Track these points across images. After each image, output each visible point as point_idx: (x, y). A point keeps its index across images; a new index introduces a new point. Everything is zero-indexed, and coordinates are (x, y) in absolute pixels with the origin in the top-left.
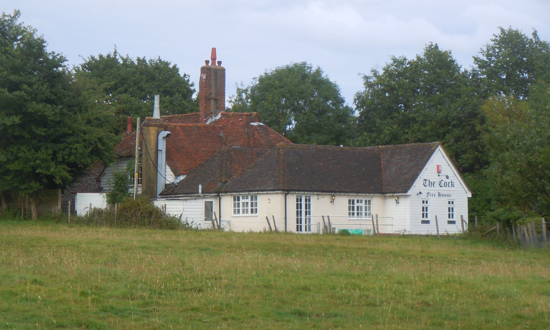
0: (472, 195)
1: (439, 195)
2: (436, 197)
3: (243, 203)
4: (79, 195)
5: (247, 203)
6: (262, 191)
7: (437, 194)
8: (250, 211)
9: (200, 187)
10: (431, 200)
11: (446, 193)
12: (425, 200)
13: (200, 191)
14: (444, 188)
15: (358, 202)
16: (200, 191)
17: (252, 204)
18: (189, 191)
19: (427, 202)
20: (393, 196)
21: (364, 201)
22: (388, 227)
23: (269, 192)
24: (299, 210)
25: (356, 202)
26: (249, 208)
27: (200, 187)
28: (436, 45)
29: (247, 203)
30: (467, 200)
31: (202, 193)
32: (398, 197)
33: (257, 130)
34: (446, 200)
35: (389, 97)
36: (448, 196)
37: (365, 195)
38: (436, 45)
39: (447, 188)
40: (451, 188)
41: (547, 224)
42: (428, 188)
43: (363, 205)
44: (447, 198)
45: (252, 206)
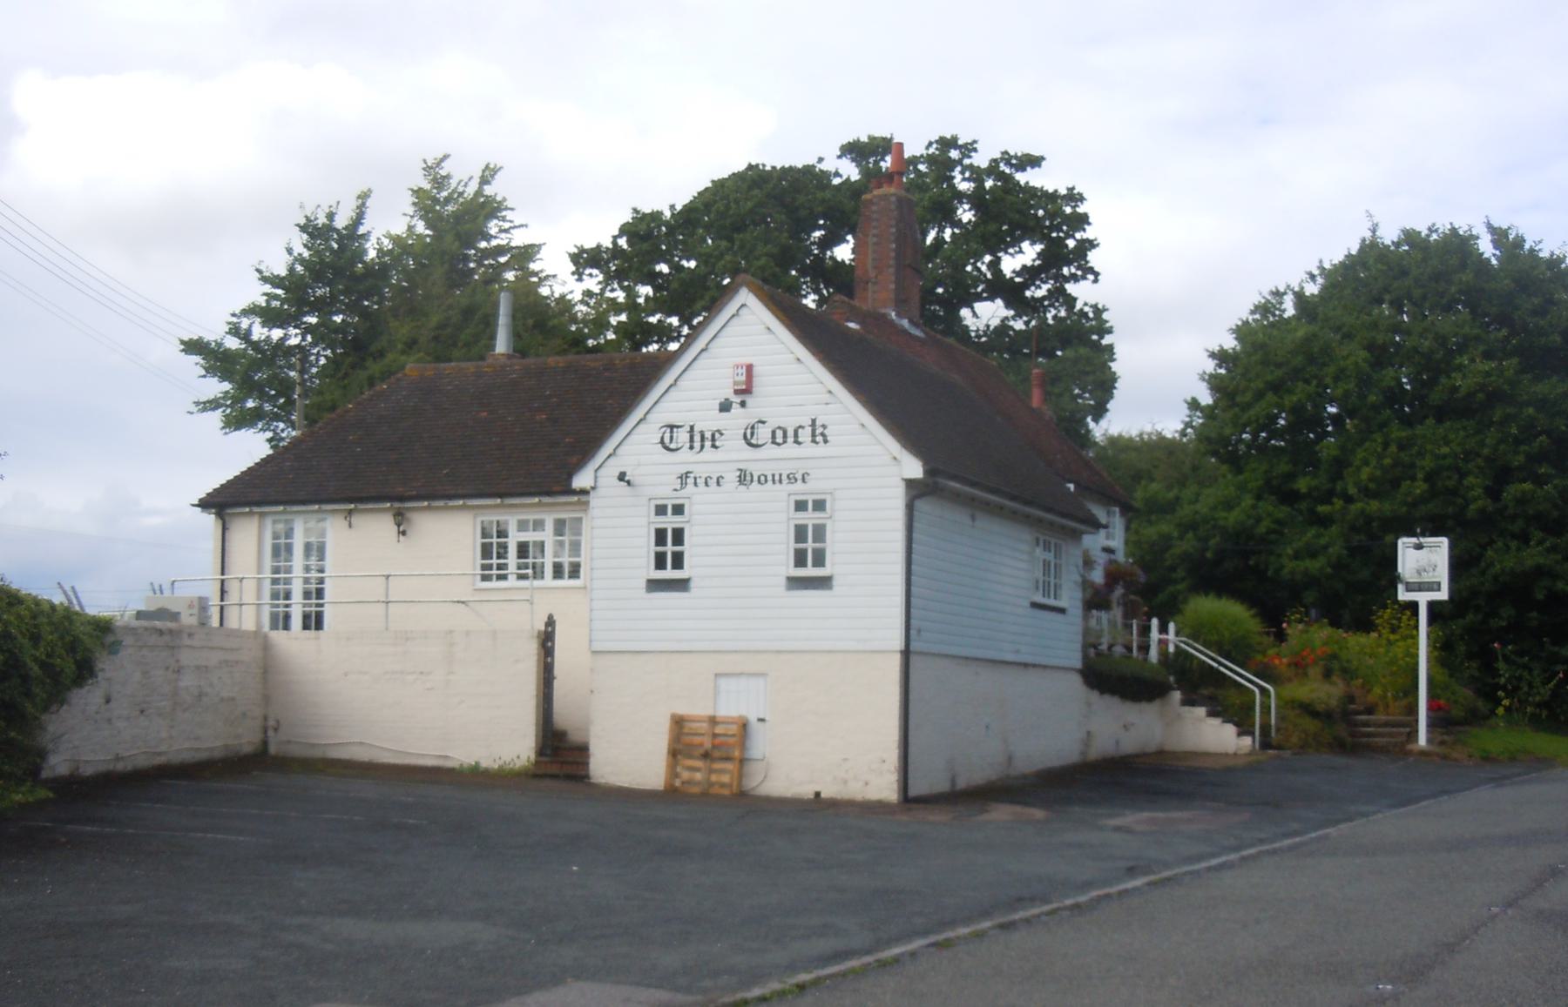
0: (926, 472)
1: (743, 478)
6: (303, 502)
7: (731, 477)
10: (699, 502)
11: (785, 469)
12: (670, 503)
14: (770, 451)
19: (678, 510)
20: (251, 513)
23: (451, 503)
28: (1213, 355)
32: (350, 512)
34: (778, 500)
35: (946, 291)
36: (792, 478)
38: (1213, 355)
39: (790, 449)
40: (808, 449)
41: (746, 1002)
42: (685, 455)
43: (547, 536)
44: (786, 487)
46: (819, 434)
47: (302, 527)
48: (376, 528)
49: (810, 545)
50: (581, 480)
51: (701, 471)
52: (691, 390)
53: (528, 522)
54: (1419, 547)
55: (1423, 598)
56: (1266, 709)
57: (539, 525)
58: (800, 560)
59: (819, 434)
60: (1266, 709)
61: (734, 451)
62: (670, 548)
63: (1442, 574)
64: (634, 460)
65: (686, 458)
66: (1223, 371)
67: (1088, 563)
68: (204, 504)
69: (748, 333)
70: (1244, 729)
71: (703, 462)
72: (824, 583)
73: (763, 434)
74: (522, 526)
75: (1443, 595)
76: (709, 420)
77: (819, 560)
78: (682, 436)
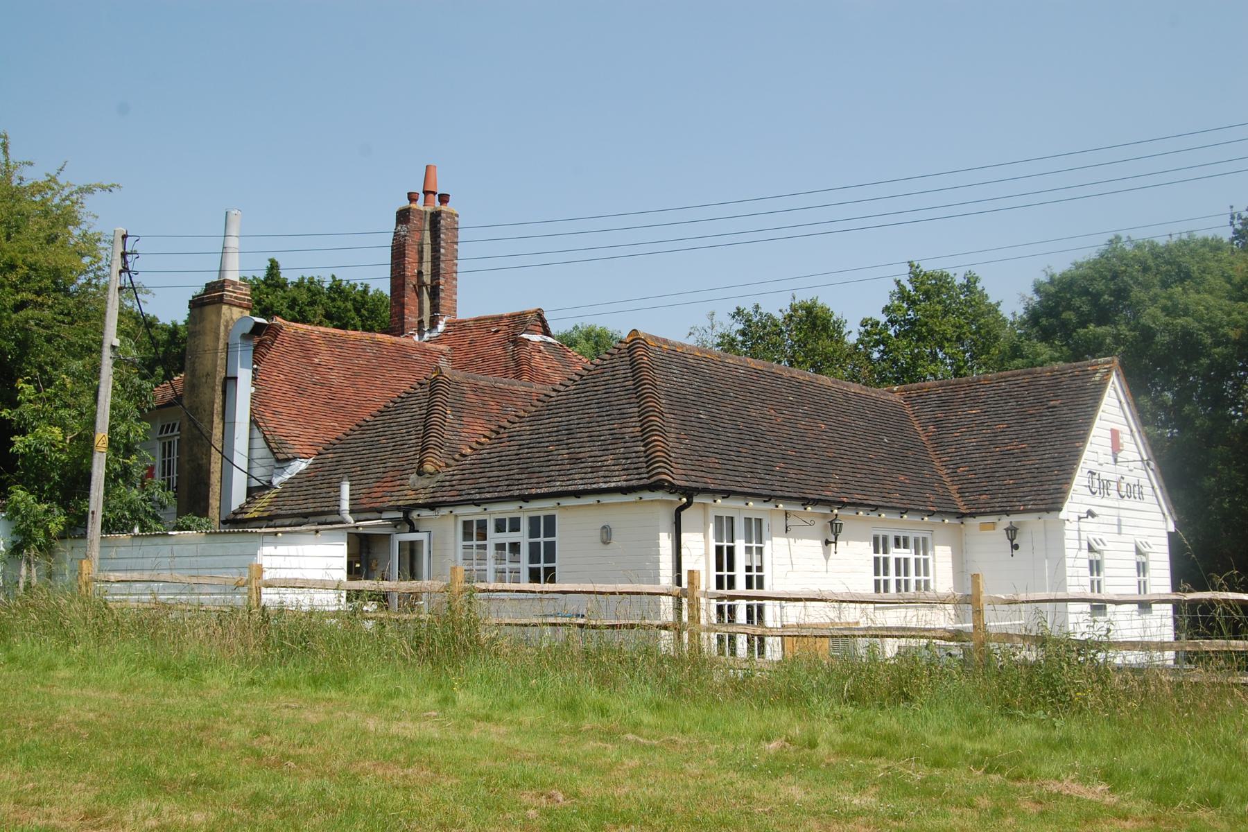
2: (1111, 535)
3: (501, 547)
4: (949, 548)
5: (515, 547)
8: (525, 574)
9: (346, 489)
13: (345, 505)
15: (500, 527)
16: (345, 505)
17: (534, 548)
18: (310, 507)
21: (525, 526)
22: (1072, 607)
24: (725, 573)
25: (491, 527)
26: (524, 565)
27: (346, 489)
29: (515, 547)
30: (1165, 541)
31: (351, 512)
33: (540, 351)
37: (216, 457)
45: (534, 557)
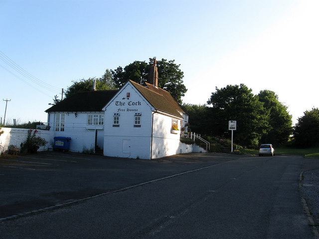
7: (126, 110)
34: (133, 114)
40: (138, 106)
46: (139, 104)
47: (60, 114)
48: (72, 115)
49: (138, 120)
50: (104, 109)
51: (121, 109)
52: (120, 97)
53: (94, 115)
54: (232, 122)
55: (232, 130)
56: (208, 145)
57: (97, 116)
58: (136, 123)
59: (139, 104)
60: (208, 145)
61: (126, 106)
62: (138, 120)
63: (235, 126)
64: (111, 108)
65: (119, 107)
66: (124, 71)
67: (262, 113)
68: (46, 111)
69: (129, 87)
70: (205, 149)
71: (122, 107)
72: (140, 126)
73: (131, 103)
74: (95, 116)
75: (235, 129)
76: (123, 101)
77: (118, 123)
78: (119, 103)
